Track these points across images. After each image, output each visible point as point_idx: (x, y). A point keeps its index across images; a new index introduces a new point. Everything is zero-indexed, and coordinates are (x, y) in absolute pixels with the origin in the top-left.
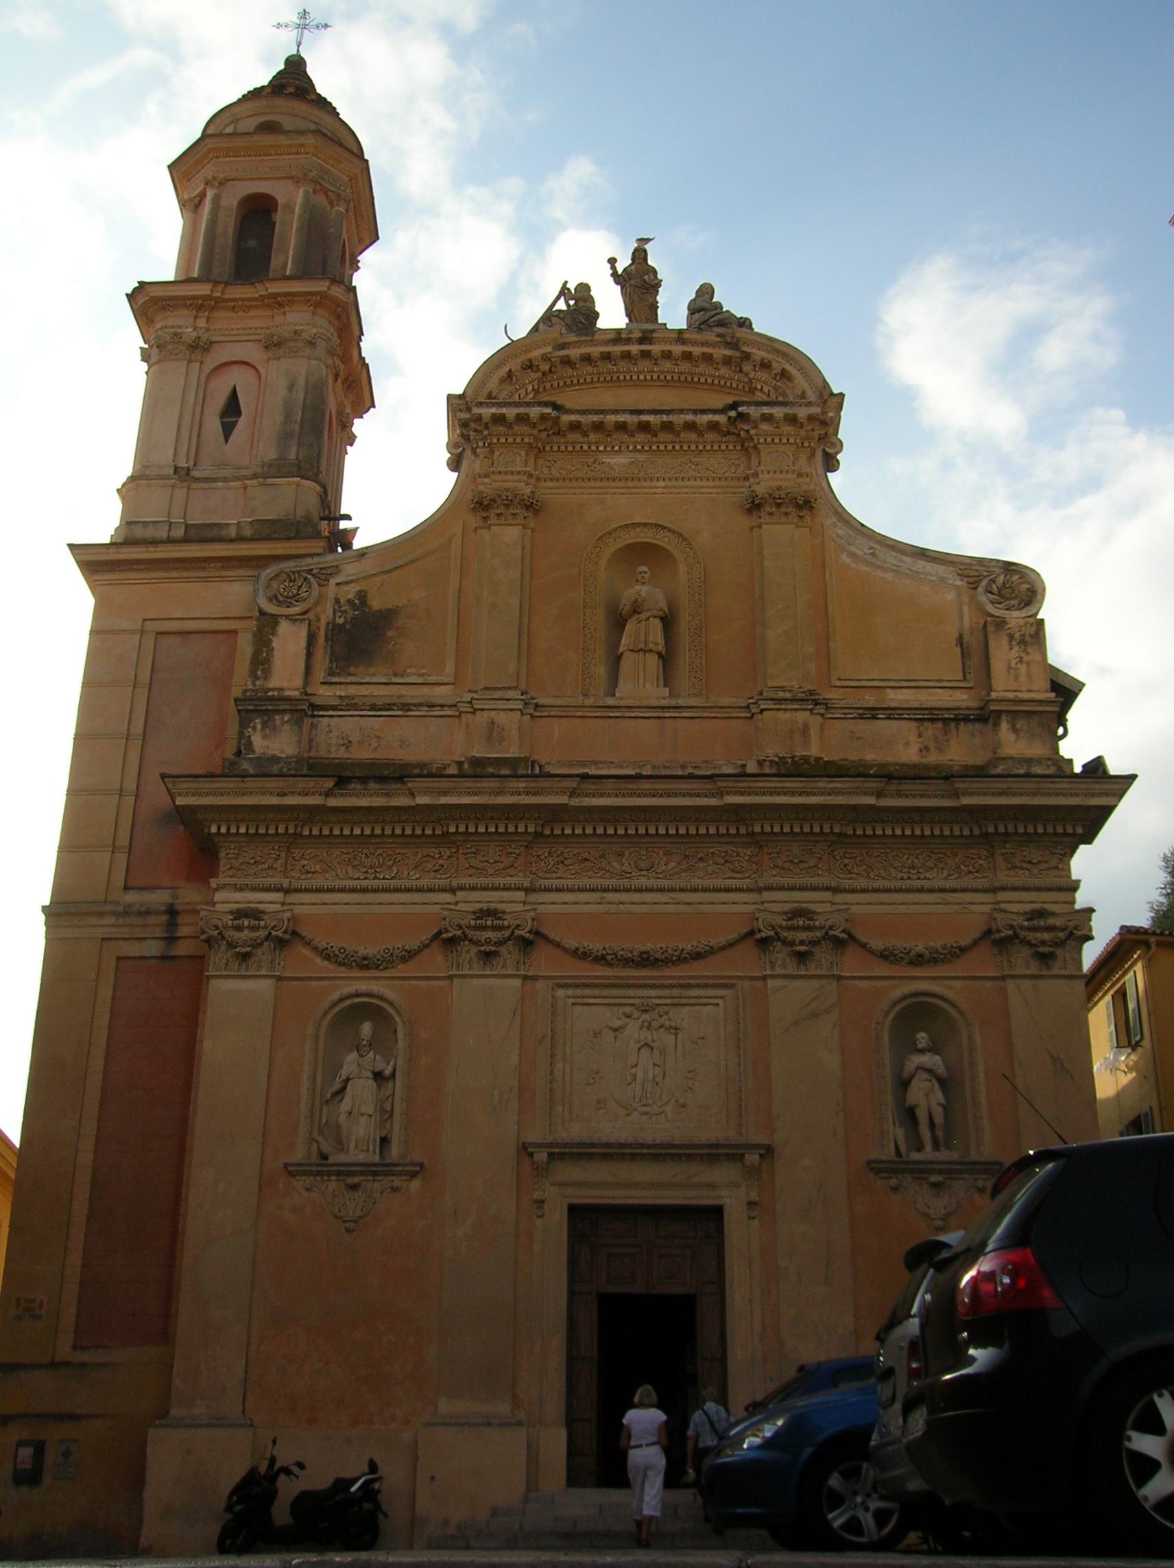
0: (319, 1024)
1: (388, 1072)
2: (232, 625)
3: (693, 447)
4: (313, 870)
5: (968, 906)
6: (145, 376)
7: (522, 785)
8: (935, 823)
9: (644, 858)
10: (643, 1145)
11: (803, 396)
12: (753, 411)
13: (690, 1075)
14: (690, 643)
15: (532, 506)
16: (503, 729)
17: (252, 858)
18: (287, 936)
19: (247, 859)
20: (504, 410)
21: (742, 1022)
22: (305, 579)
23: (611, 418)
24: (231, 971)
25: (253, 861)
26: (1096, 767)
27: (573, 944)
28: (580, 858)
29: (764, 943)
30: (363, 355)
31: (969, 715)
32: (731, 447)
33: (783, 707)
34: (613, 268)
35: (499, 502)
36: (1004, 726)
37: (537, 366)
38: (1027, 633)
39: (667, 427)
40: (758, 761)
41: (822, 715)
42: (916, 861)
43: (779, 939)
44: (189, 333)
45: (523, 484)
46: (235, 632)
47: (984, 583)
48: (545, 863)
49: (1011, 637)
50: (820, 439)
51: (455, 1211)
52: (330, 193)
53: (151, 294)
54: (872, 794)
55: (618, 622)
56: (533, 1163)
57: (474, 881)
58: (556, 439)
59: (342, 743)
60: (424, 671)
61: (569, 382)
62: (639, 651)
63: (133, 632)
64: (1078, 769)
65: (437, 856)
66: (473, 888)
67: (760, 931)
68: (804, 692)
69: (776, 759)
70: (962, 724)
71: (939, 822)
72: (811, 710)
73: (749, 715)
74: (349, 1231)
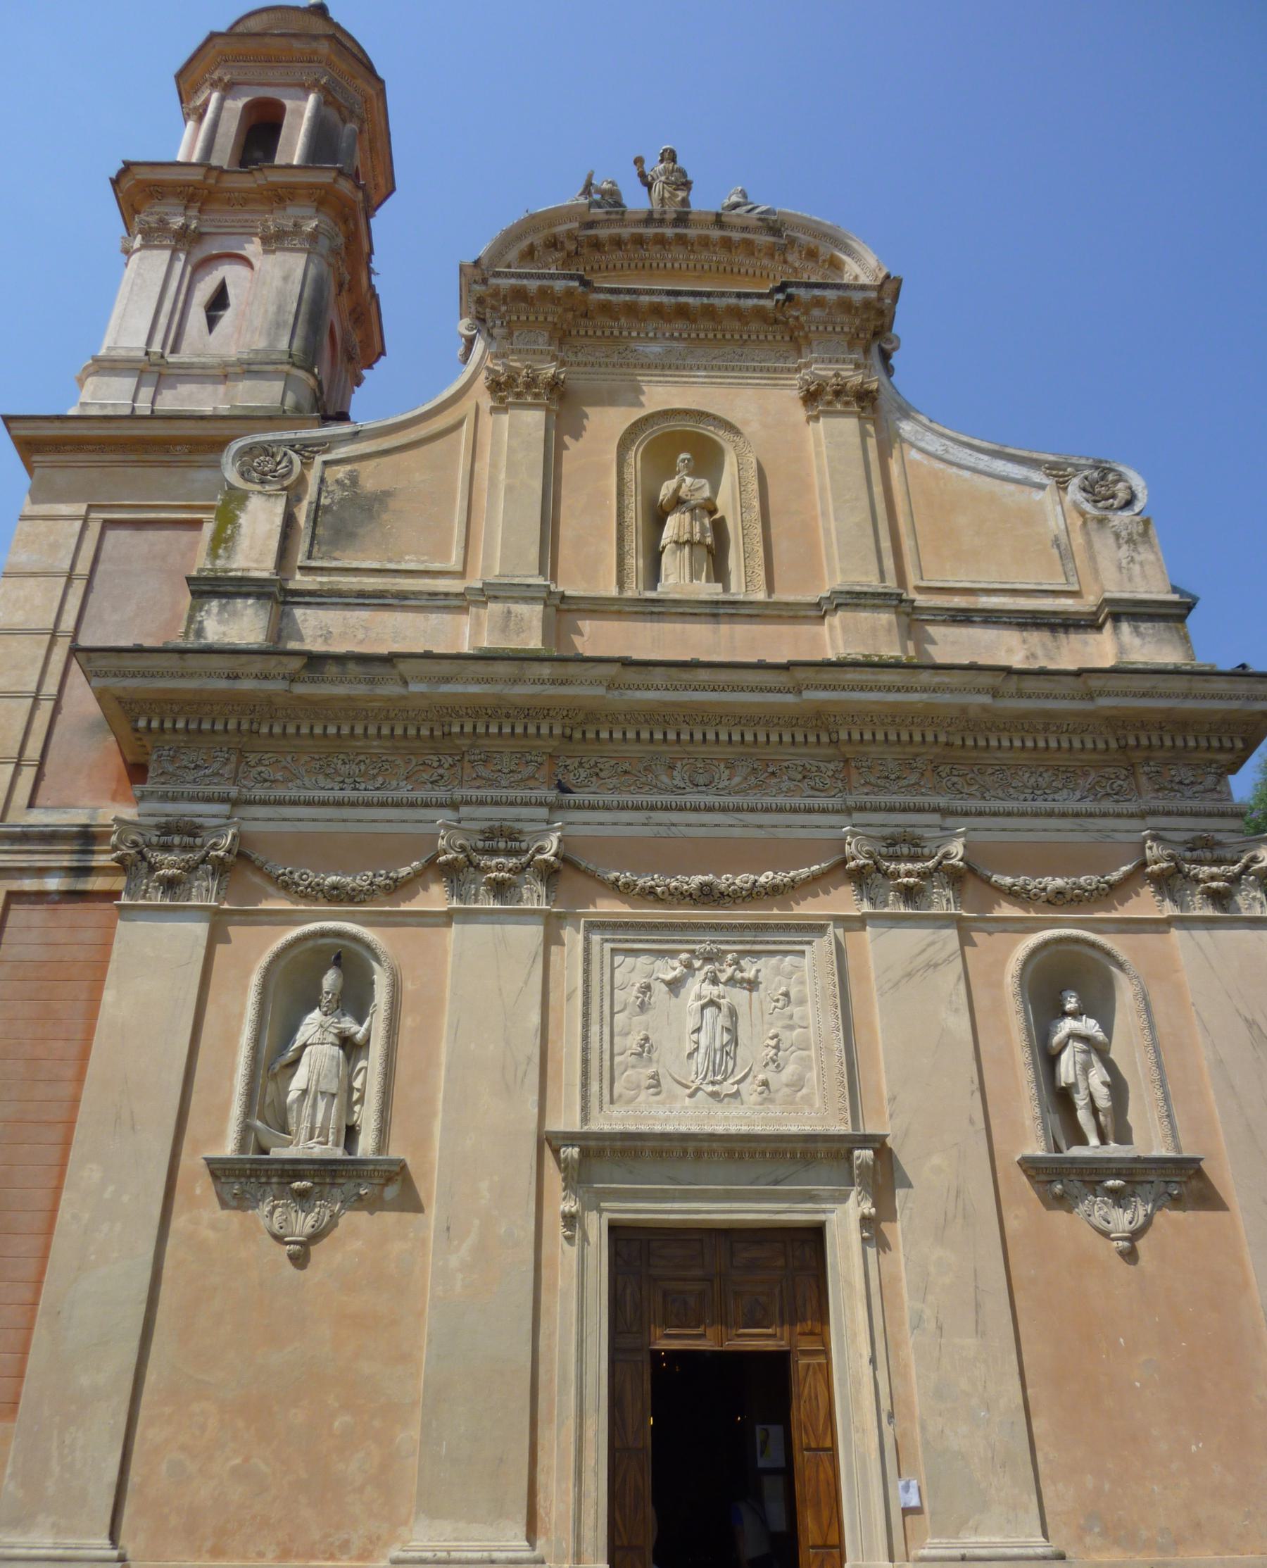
3: (737, 337)
4: (272, 778)
5: (1110, 834)
8: (1062, 733)
9: (701, 771)
12: (802, 293)
16: (522, 619)
17: (192, 762)
18: (230, 859)
19: (185, 763)
23: (645, 299)
24: (150, 899)
25: (193, 765)
28: (620, 769)
31: (1081, 620)
32: (778, 337)
38: (1135, 531)
42: (1040, 779)
43: (879, 870)
48: (575, 775)
49: (1117, 536)
51: (448, 1229)
52: (343, 109)
53: (138, 177)
54: (988, 692)
55: (657, 517)
57: (481, 793)
58: (583, 321)
59: (320, 633)
60: (426, 558)
61: (596, 267)
65: (436, 764)
66: (481, 803)
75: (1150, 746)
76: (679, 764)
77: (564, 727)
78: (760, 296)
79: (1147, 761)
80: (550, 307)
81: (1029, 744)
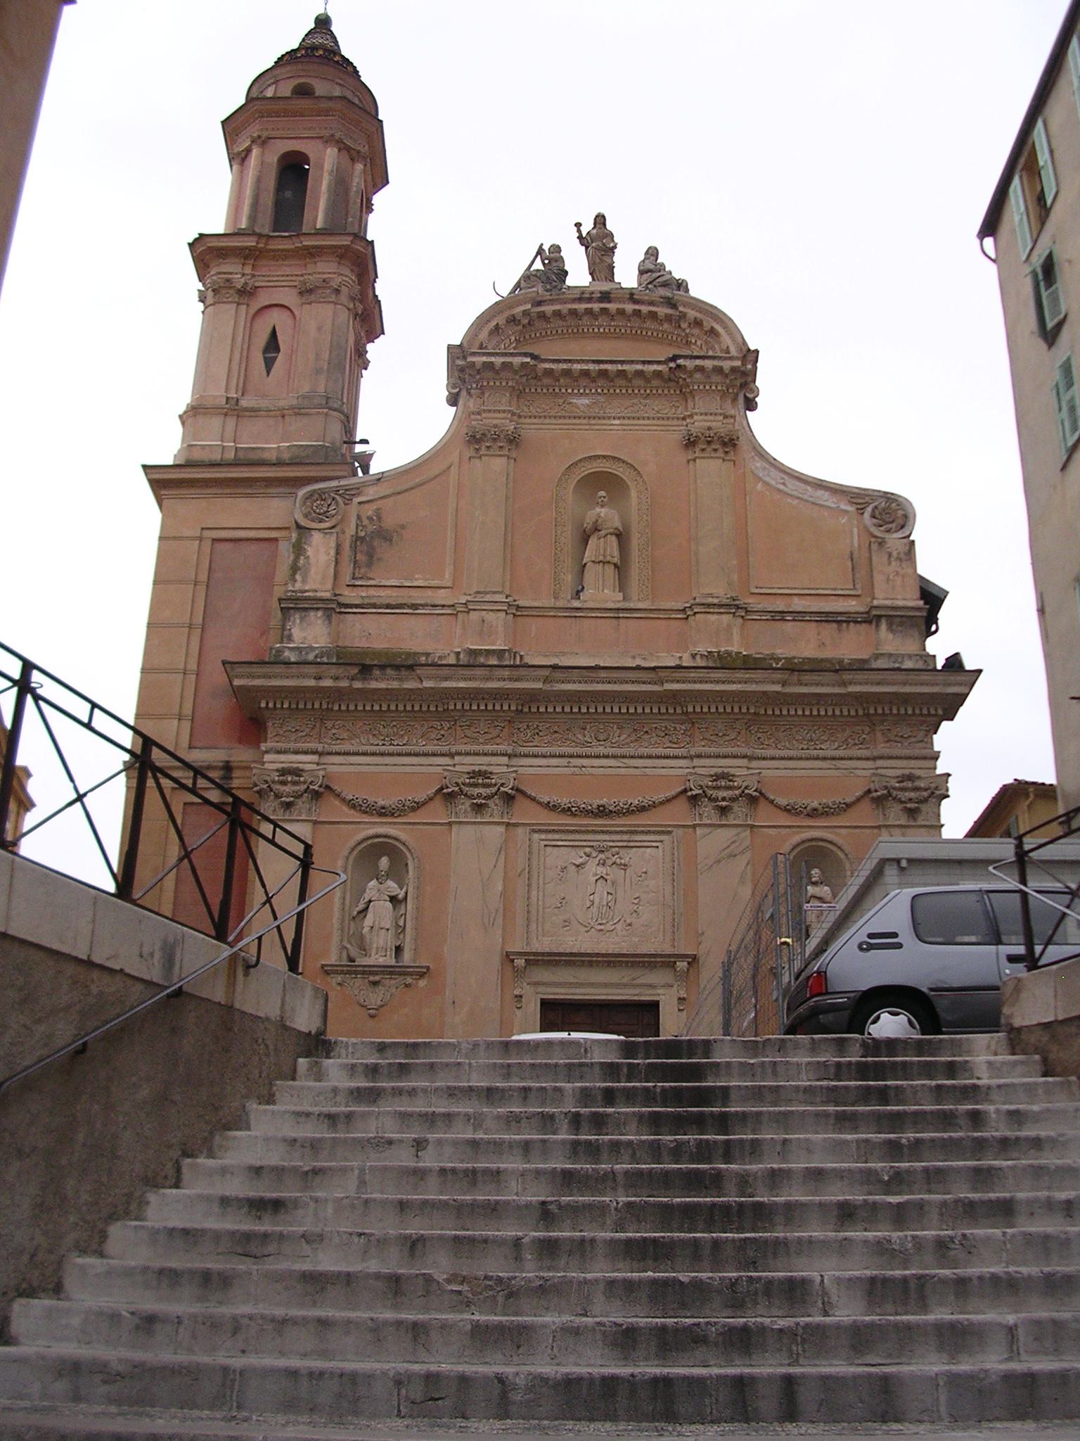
0: (347, 858)
1: (400, 897)
2: (273, 534)
4: (341, 737)
6: (201, 315)
7: (506, 673)
10: (598, 955)
11: (728, 352)
12: (689, 364)
13: (636, 901)
14: (639, 556)
15: (514, 441)
18: (322, 790)
20: (493, 359)
21: (676, 860)
22: (334, 499)
23: (577, 367)
26: (954, 662)
27: (546, 799)
29: (694, 800)
30: (377, 294)
33: (712, 610)
34: (579, 231)
35: (489, 436)
36: (884, 626)
37: (519, 320)
39: (622, 374)
40: (692, 655)
41: (742, 617)
43: (706, 796)
44: (239, 282)
45: (508, 421)
46: (276, 540)
47: (869, 509)
49: (890, 555)
50: (741, 385)
53: (209, 245)
56: (514, 967)
57: (468, 748)
58: (533, 382)
62: (599, 562)
63: (194, 538)
64: (940, 664)
66: (468, 754)
67: (691, 790)
68: (728, 598)
69: (706, 653)
70: (852, 625)
71: (831, 704)
72: (734, 613)
73: (685, 616)
74: (372, 1016)
75: (884, 714)
76: (588, 727)
77: (517, 705)
78: (659, 363)
79: (882, 722)
80: (510, 375)
81: (807, 713)
